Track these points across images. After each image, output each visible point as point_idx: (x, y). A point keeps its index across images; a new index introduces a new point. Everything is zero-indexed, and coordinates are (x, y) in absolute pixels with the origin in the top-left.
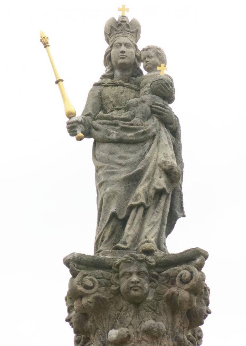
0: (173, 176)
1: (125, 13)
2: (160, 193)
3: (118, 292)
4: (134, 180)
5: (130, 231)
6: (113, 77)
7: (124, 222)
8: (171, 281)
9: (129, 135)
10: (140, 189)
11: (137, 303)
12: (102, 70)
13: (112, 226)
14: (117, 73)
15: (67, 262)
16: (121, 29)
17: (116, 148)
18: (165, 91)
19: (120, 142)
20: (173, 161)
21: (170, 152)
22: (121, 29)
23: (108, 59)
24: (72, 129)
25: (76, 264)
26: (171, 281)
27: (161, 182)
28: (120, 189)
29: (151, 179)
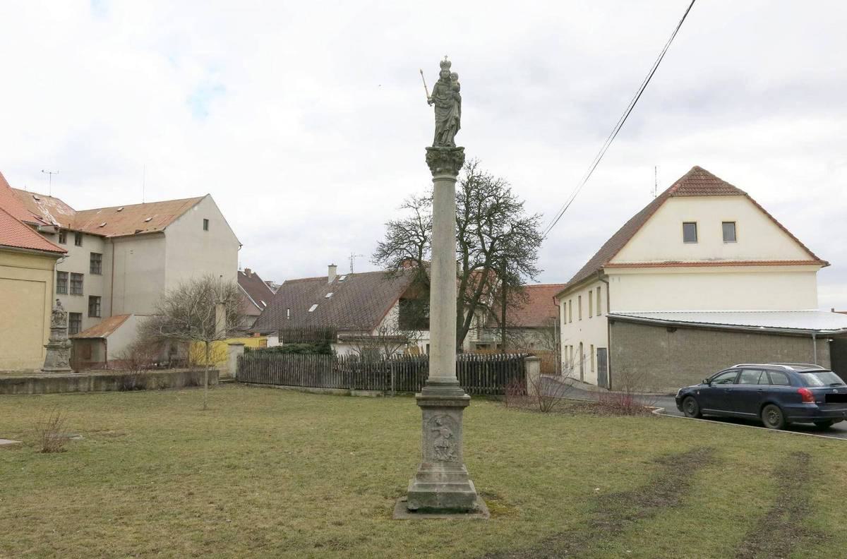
0: (458, 120)
1: (272, 346)
2: (453, 126)
3: (439, 158)
4: (446, 122)
5: (444, 138)
6: (461, 404)
7: (443, 134)
8: (454, 155)
9: (446, 106)
10: (447, 125)
11: (445, 161)
12: (439, 77)
13: (439, 136)
14: (443, 80)
15: (426, 149)
16: (445, 65)
17: (441, 110)
18: (457, 90)
19: (443, 108)
20: (458, 115)
21: (457, 111)
22: (445, 65)
23: (440, 74)
24: (429, 103)
25: (429, 149)
26: (454, 155)
27: (453, 122)
28: (442, 124)
29: (451, 121)
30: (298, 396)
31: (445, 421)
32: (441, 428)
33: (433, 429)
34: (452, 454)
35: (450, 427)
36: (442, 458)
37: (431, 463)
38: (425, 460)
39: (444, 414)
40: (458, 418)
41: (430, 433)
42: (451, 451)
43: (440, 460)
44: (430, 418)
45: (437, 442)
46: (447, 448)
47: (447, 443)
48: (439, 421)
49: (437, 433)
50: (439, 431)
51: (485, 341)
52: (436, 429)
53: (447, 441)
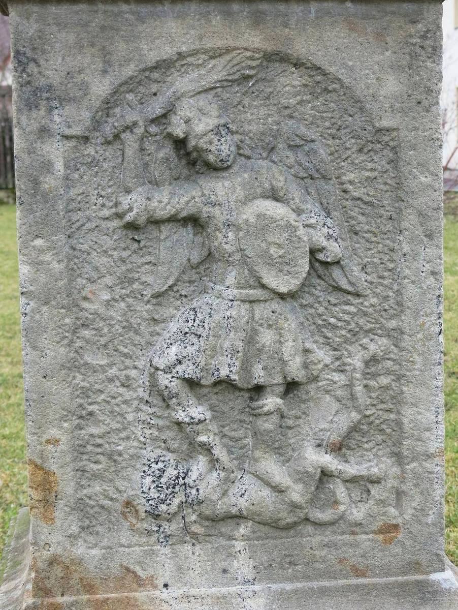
30: (357, 519)
31: (256, 118)
32: (220, 188)
33: (136, 203)
34: (338, 449)
35: (312, 177)
36: (248, 494)
37: (129, 544)
38: (65, 520)
39: (254, 39)
40: (392, 85)
41: (105, 249)
42: (328, 418)
43: (221, 521)
44: (101, 88)
45: (206, 329)
46: (291, 387)
47: (290, 342)
48: (199, 121)
49: (177, 248)
50: (194, 222)
51: (175, 21)
52: (168, 200)
53: (290, 320)
